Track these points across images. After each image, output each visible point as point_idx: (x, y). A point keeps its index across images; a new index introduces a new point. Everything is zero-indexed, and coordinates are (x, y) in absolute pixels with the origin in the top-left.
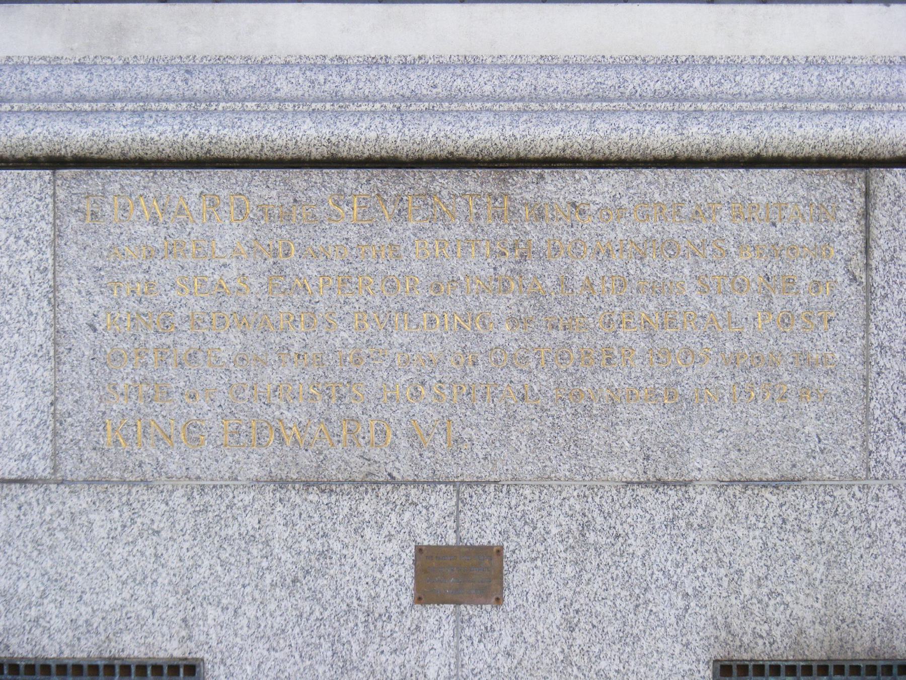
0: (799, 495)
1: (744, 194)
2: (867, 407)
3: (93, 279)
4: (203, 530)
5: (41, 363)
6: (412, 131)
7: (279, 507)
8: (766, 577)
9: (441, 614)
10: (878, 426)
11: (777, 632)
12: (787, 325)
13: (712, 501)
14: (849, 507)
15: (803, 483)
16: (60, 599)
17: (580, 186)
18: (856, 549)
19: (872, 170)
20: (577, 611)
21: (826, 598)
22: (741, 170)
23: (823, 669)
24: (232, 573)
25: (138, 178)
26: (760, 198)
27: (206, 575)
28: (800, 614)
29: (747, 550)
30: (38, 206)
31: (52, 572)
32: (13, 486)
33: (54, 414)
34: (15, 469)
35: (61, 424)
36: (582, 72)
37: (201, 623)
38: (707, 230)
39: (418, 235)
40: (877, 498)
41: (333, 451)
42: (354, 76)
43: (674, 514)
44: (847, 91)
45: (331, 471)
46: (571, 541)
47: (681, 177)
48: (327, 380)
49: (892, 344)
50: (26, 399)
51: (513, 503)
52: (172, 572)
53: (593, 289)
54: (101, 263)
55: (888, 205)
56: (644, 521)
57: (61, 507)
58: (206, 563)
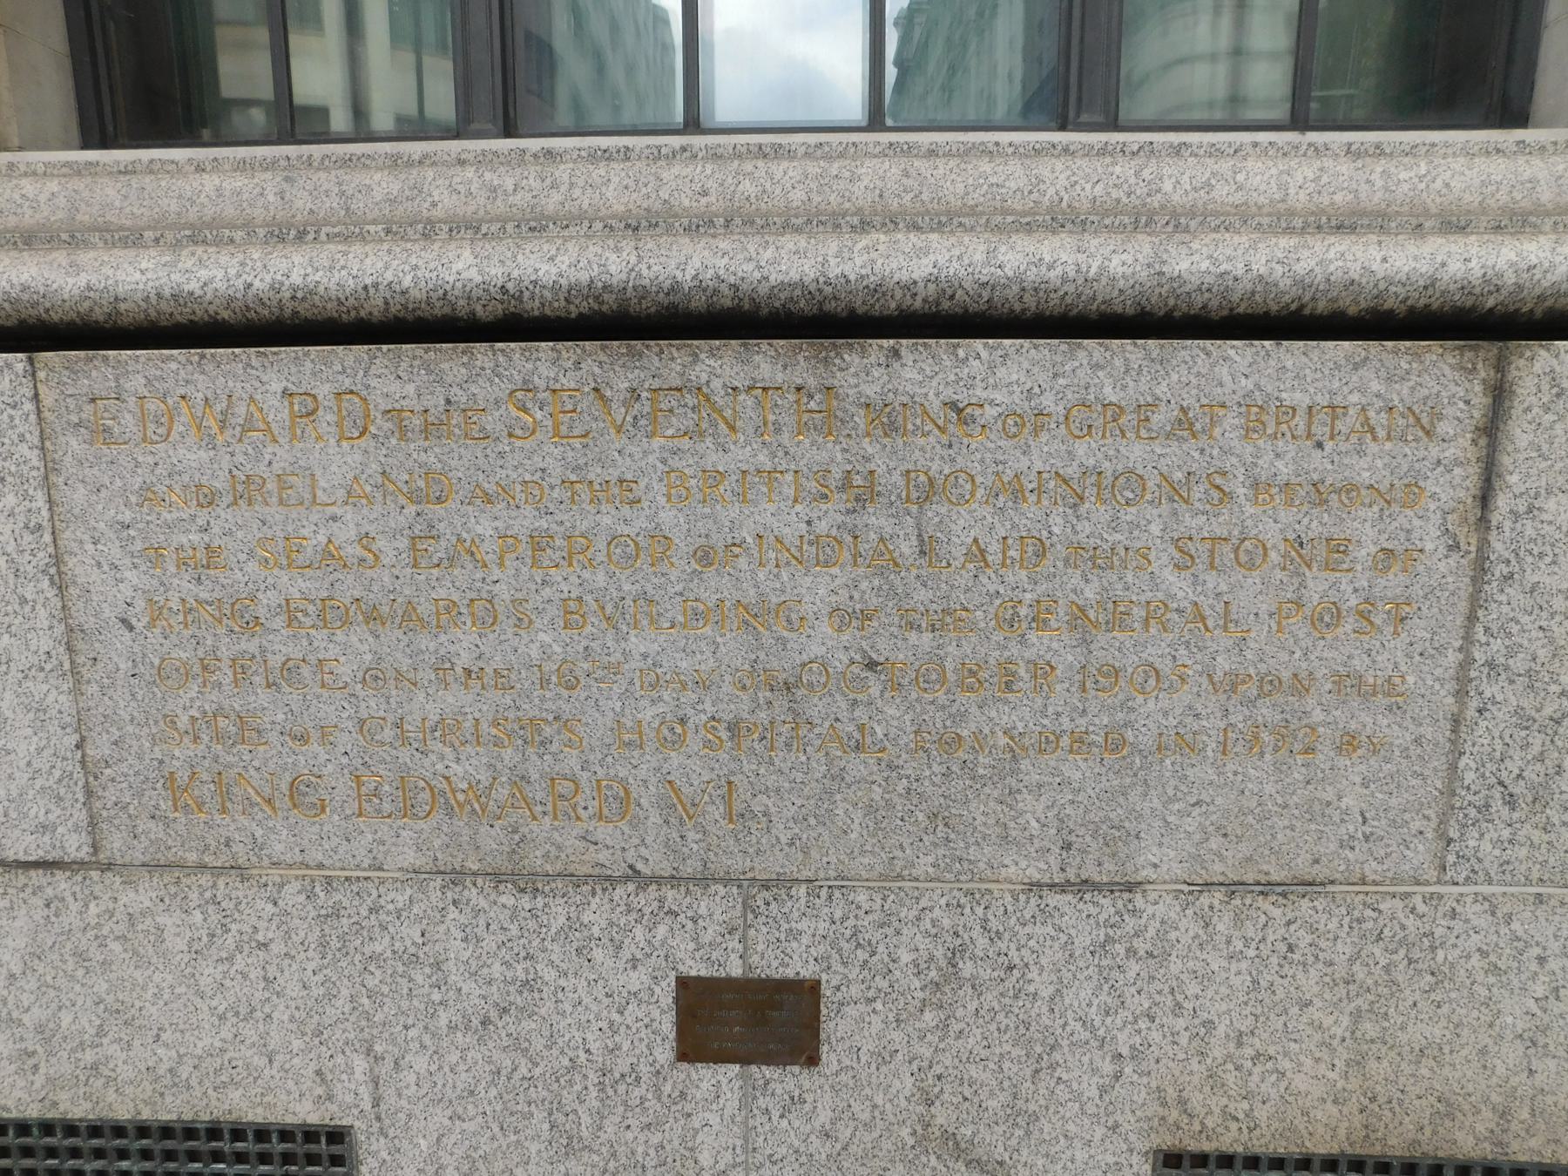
0: (1320, 908)
1: (1269, 389)
2: (1453, 767)
3: (117, 543)
4: (335, 944)
5: (51, 681)
6: (655, 268)
7: (453, 913)
8: (1252, 1033)
9: (720, 1077)
10: (1469, 798)
11: (1262, 1113)
12: (1328, 625)
13: (1172, 914)
14: (1403, 927)
15: (1330, 888)
16: (126, 1038)
17: (966, 370)
18: (1408, 992)
19: (1513, 344)
20: (939, 1078)
21: (1348, 1065)
22: (1266, 343)
23: (1331, 1164)
24: (386, 1009)
25: (174, 366)
26: (1298, 395)
27: (346, 1010)
28: (1302, 1088)
29: (1224, 990)
30: (12, 418)
31: (110, 999)
32: (33, 873)
33: (83, 762)
34: (33, 846)
35: (96, 778)
36: (963, 166)
37: (344, 1077)
38: (1196, 455)
39: (670, 462)
40: (1454, 914)
41: (535, 828)
42: (566, 177)
43: (1107, 935)
44: (1438, 200)
45: (535, 859)
46: (933, 973)
47: (1154, 355)
48: (520, 714)
49: (1511, 661)
50: (35, 739)
51: (838, 914)
52: (293, 1004)
53: (985, 560)
54: (127, 516)
55: (1535, 410)
56: (1056, 945)
57: (111, 906)
58: (345, 992)
